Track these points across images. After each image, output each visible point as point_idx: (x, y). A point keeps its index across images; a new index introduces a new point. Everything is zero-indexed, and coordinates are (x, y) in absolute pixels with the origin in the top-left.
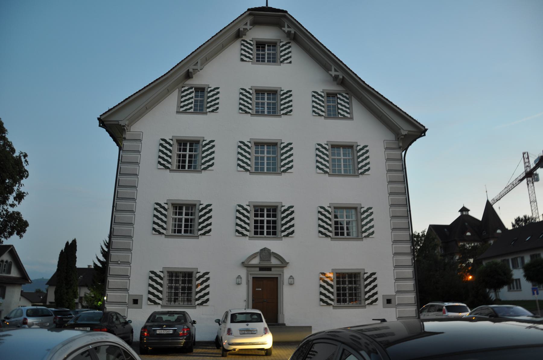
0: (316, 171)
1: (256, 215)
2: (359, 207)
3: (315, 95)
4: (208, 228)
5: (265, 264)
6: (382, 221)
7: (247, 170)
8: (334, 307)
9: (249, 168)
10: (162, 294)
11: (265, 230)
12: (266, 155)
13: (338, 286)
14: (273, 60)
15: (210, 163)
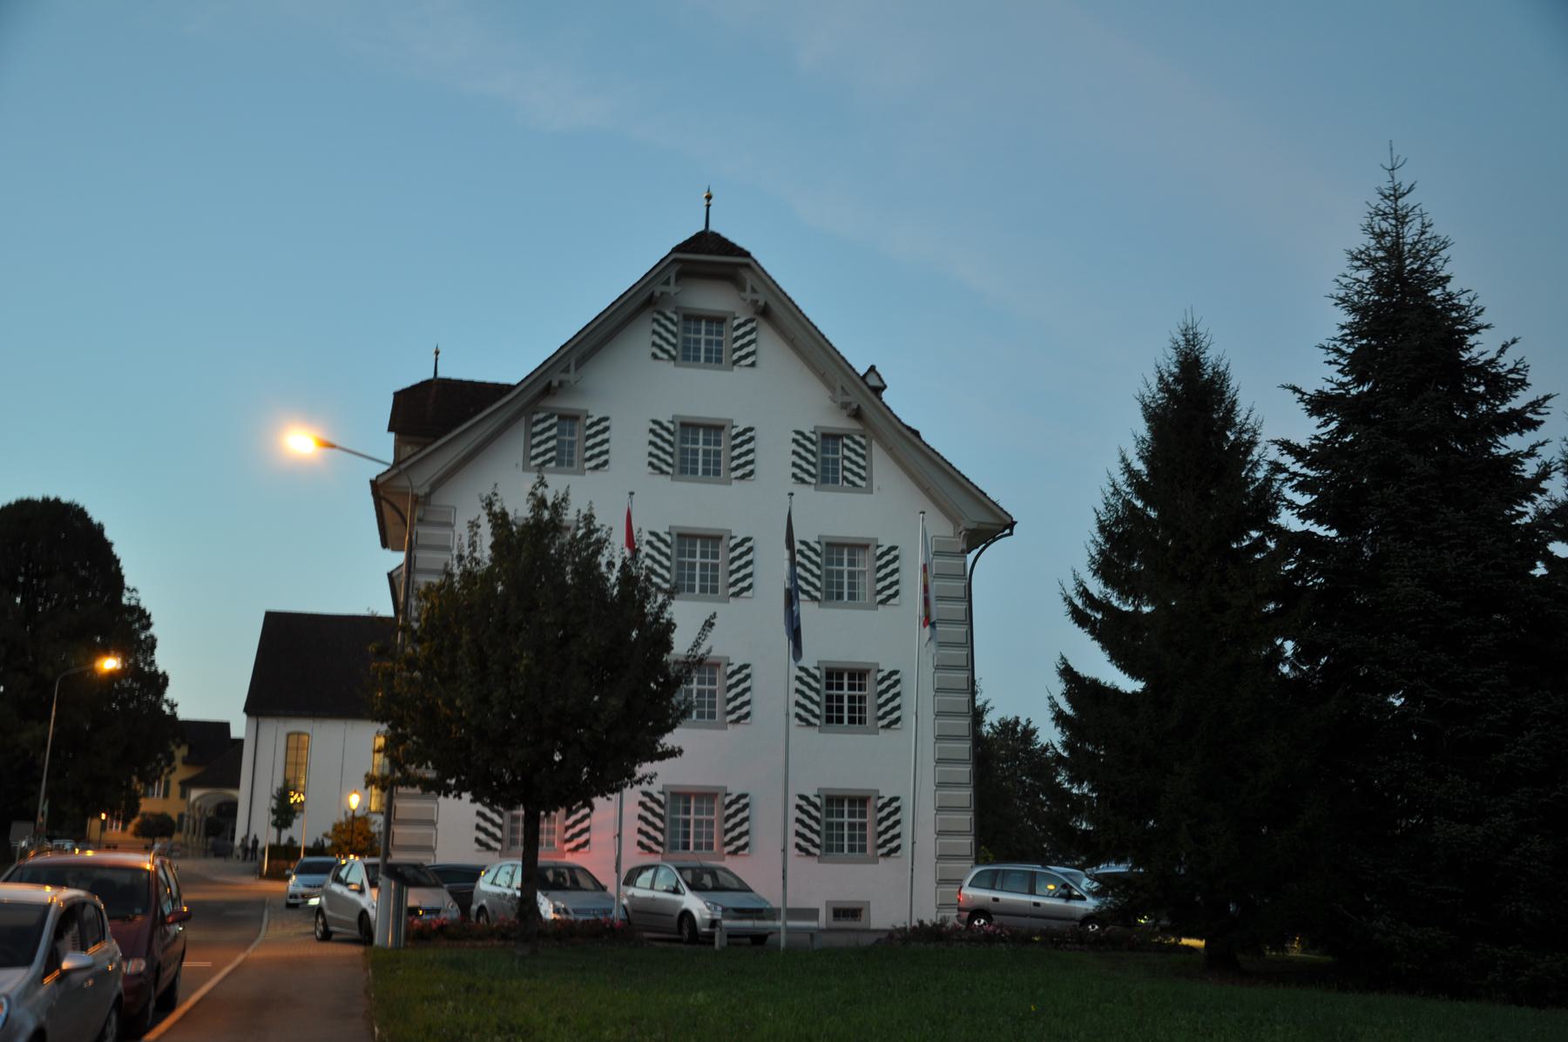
1: (829, 686)
3: (800, 438)
4: (895, 715)
6: (919, 696)
11: (846, 715)
12: (698, 560)
14: (715, 358)
15: (745, 584)
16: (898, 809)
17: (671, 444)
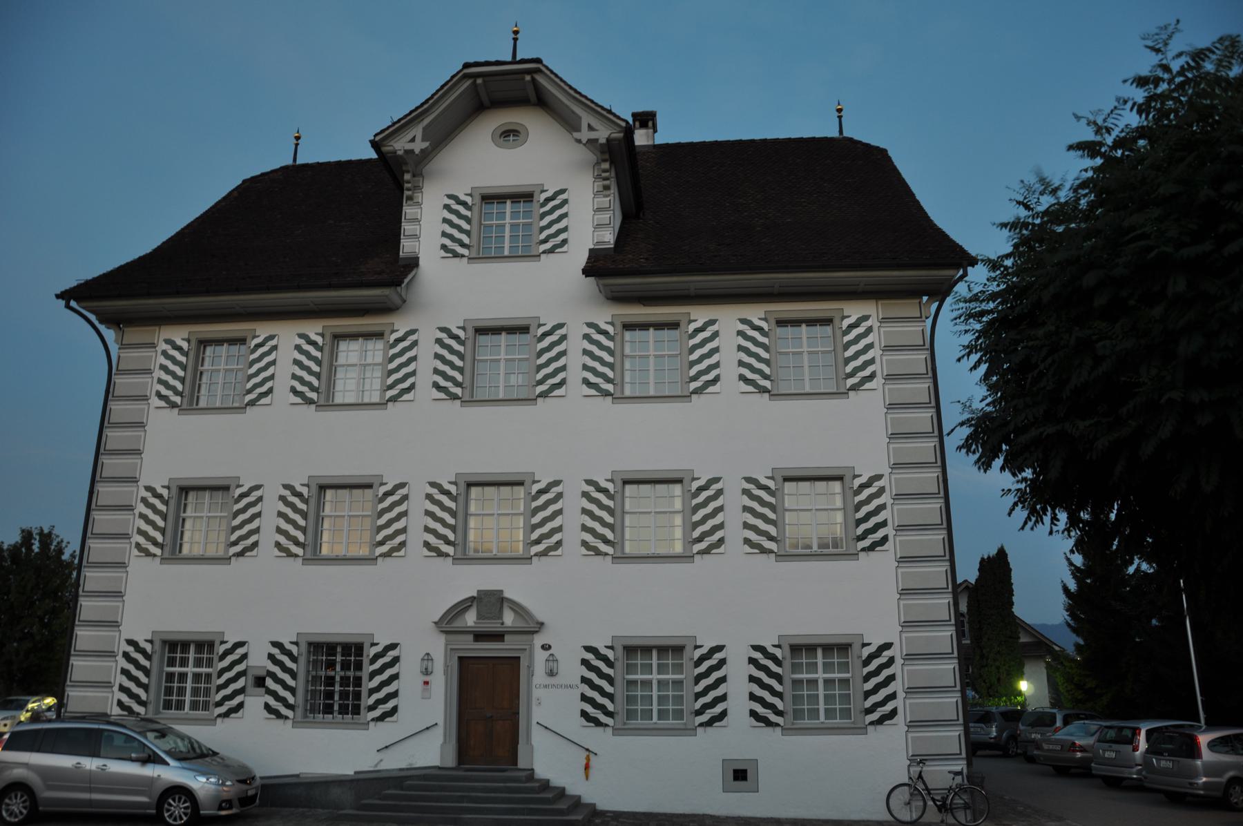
2: (376, 482)
5: (490, 626)
8: (296, 724)
10: (612, 701)
13: (358, 674)
15: (710, 376)
16: (396, 660)
17: (468, 220)
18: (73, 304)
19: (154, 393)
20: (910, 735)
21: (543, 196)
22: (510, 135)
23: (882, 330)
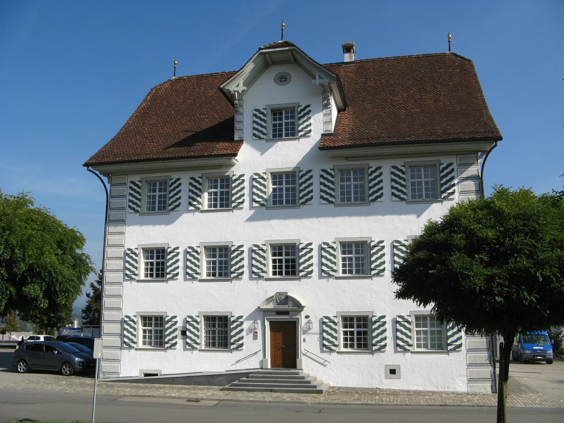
0: (392, 198)
7: (403, 199)
9: (405, 197)
10: (405, 188)
15: (309, 197)
18: (90, 168)
19: (127, 206)
20: (468, 355)
21: (300, 109)
22: (283, 79)
23: (459, 170)
